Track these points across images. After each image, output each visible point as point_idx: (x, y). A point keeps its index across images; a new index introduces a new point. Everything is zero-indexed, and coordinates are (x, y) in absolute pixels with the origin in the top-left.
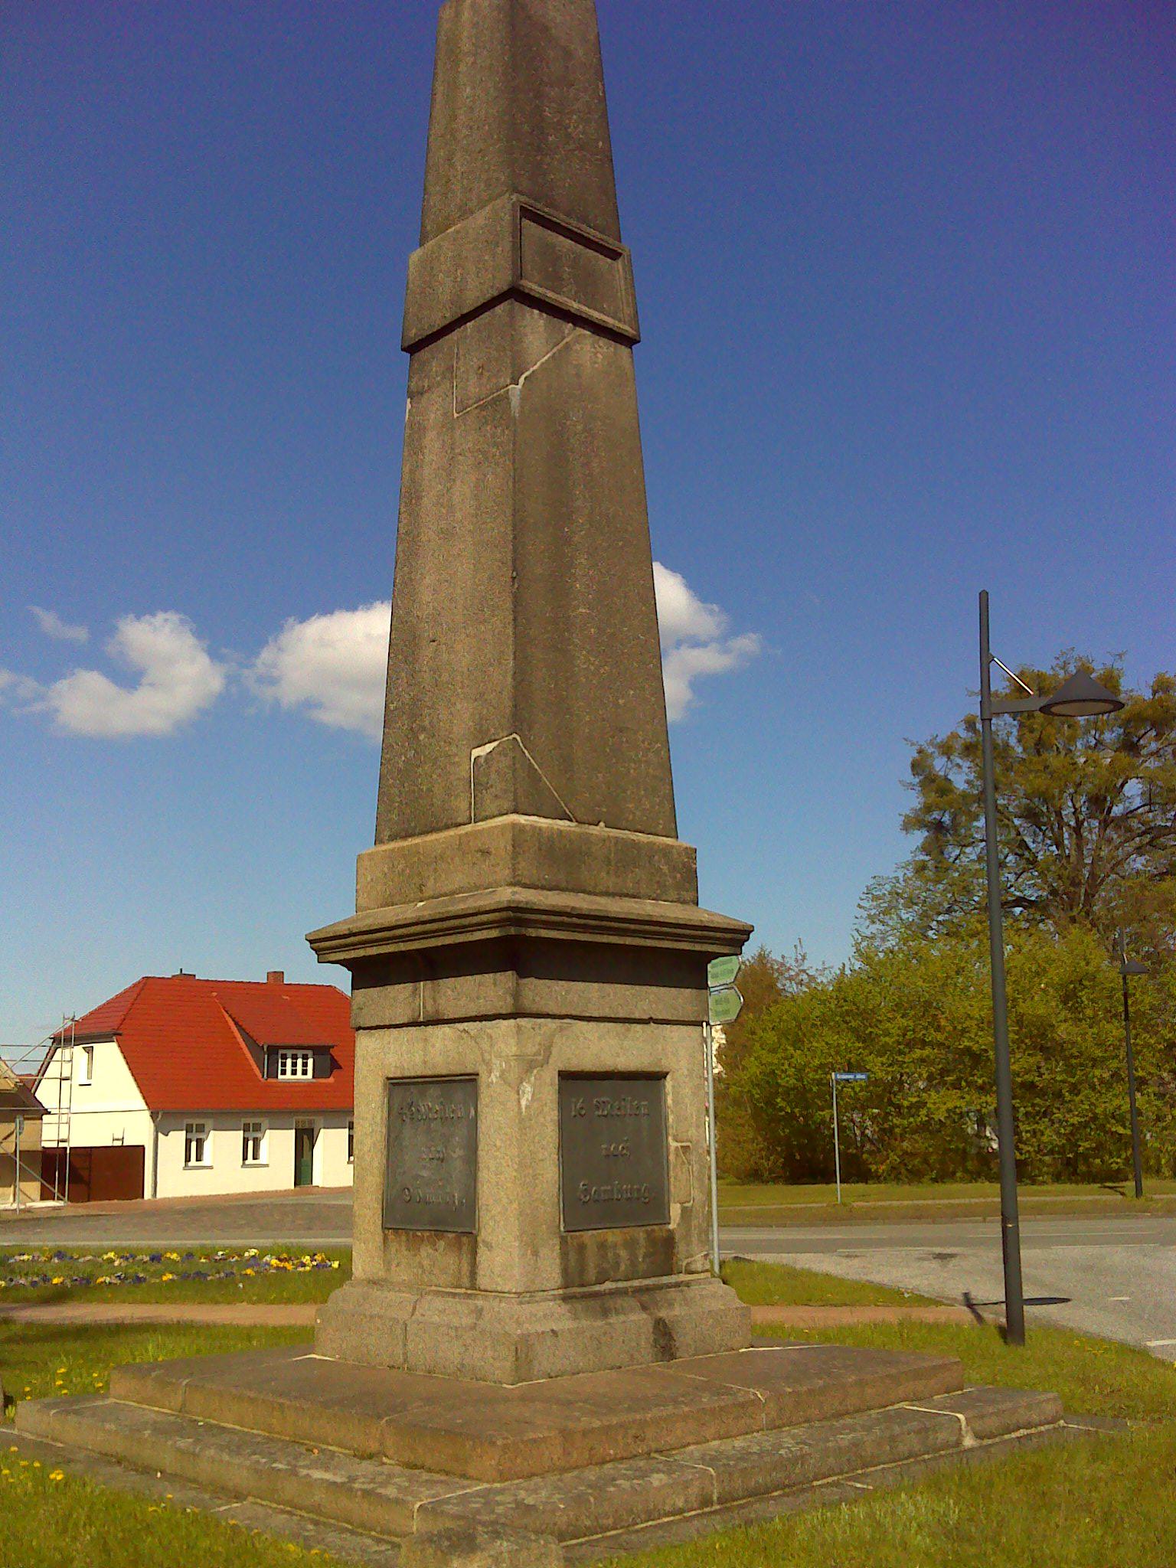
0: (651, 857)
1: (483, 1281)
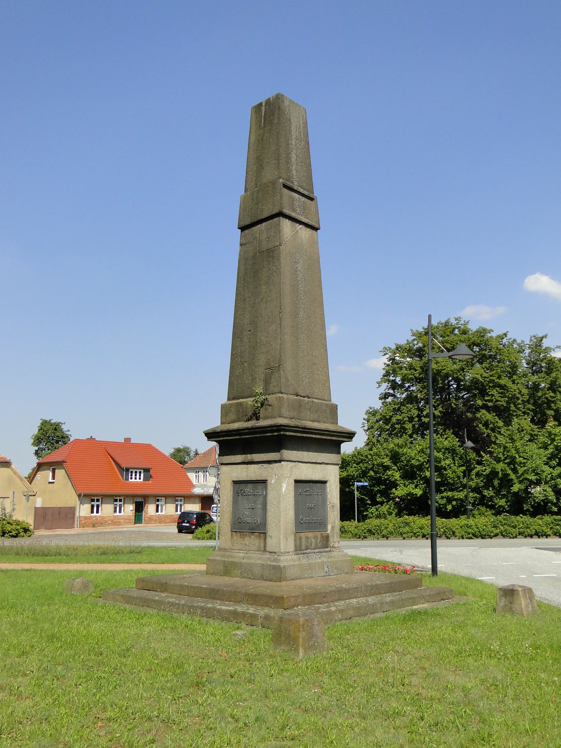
1: (268, 549)
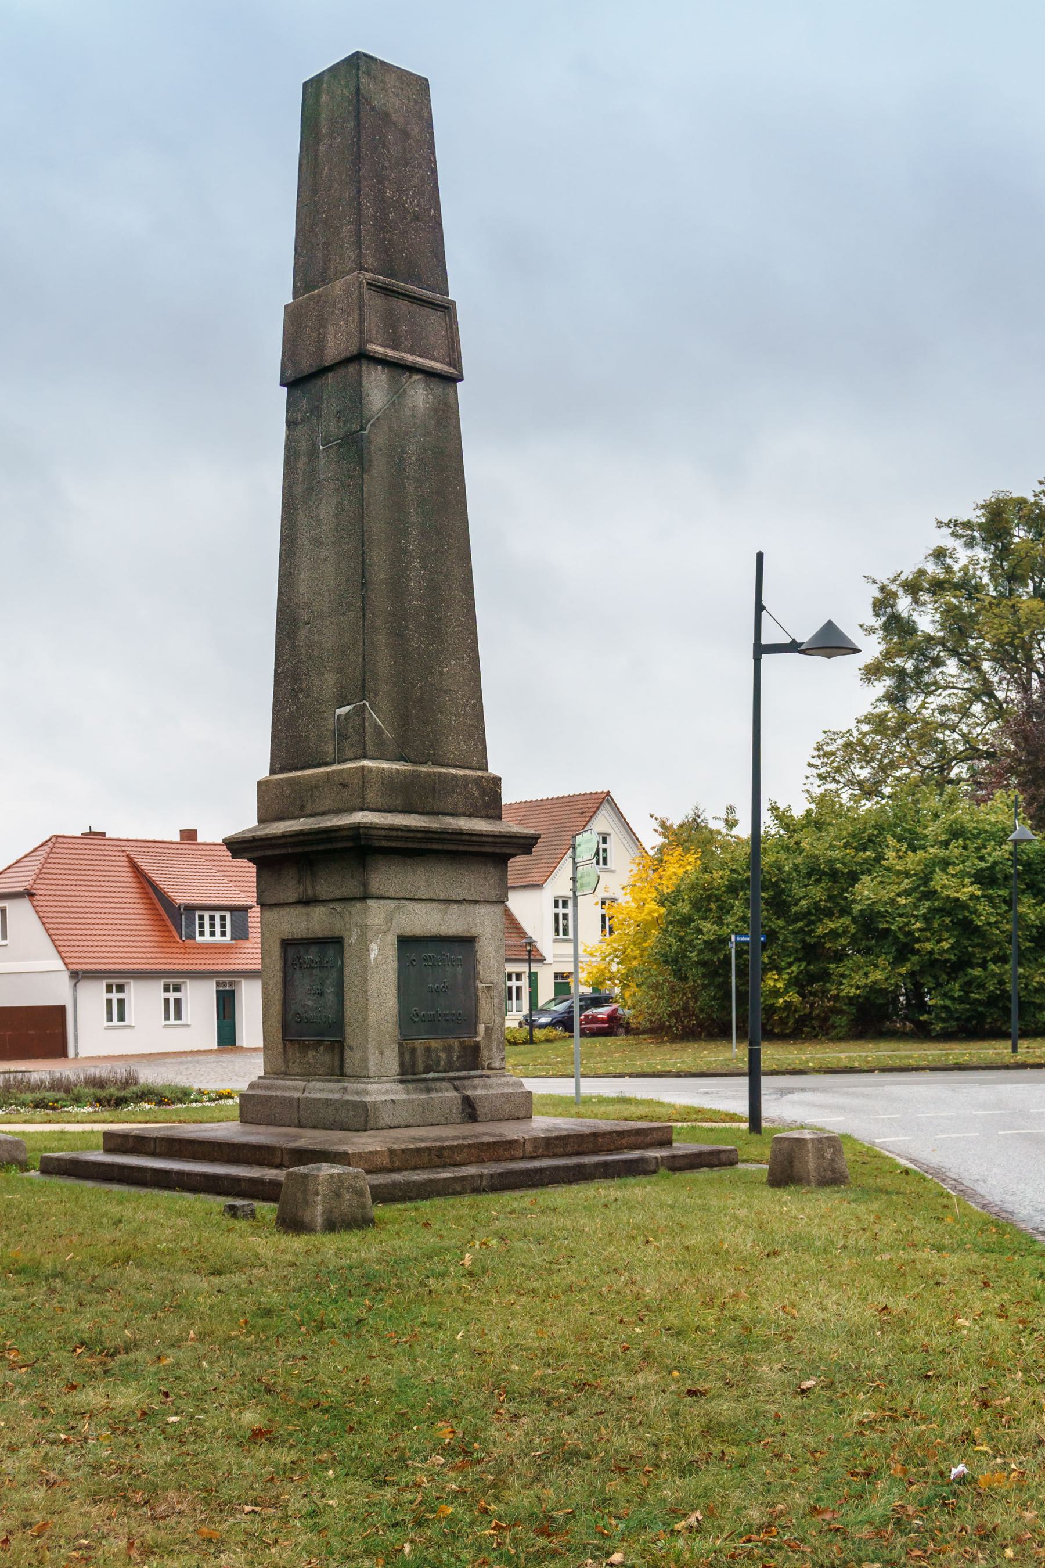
0: (466, 786)
1: (348, 1071)
